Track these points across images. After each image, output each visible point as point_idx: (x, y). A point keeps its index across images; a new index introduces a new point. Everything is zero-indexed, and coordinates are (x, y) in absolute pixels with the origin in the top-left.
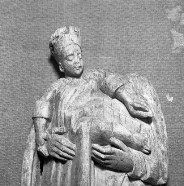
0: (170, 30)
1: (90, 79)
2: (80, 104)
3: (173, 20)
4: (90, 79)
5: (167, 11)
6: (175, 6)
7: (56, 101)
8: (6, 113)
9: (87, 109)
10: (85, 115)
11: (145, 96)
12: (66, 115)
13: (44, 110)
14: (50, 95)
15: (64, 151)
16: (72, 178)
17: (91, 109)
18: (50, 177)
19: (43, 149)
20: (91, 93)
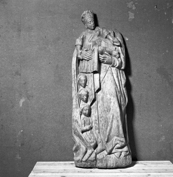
0: (128, 11)
1: (97, 31)
2: (94, 40)
3: (129, 7)
4: (97, 31)
5: (127, 3)
6: (130, 1)
7: (83, 40)
8: (64, 44)
9: (97, 42)
10: (96, 44)
11: (117, 38)
12: (108, 165)
13: (79, 42)
14: (82, 37)
15: (89, 57)
16: (126, 136)
17: (98, 42)
18: (83, 67)
19: (79, 56)
20: (98, 36)
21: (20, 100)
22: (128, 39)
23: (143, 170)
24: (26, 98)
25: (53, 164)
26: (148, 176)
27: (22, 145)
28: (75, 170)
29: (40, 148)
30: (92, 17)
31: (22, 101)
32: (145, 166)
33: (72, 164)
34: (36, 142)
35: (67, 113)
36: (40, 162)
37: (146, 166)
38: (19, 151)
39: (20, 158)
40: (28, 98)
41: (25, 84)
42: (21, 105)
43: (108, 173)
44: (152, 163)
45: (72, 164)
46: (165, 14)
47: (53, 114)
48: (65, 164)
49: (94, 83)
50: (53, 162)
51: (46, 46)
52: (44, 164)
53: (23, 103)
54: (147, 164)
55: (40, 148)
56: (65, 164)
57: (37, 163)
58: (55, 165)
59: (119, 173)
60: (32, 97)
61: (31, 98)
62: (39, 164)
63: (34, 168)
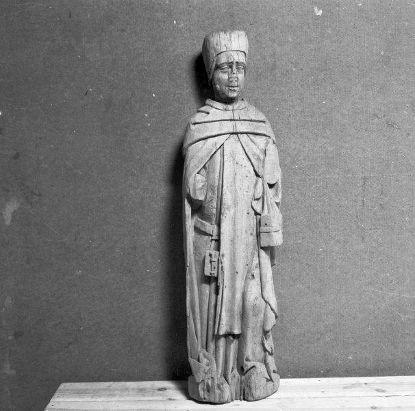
25: (105, 390)
30: (218, 67)
32: (379, 394)
36: (68, 384)
37: (383, 394)
39: (13, 372)
41: (17, 156)
42: (8, 222)
43: (250, 161)
44: (352, 386)
45: (160, 390)
49: (214, 121)
50: (107, 384)
52: (352, 386)
53: (14, 214)
55: (70, 343)
57: (62, 386)
59: (209, 329)
60: (40, 195)
62: (64, 393)
63: (49, 405)
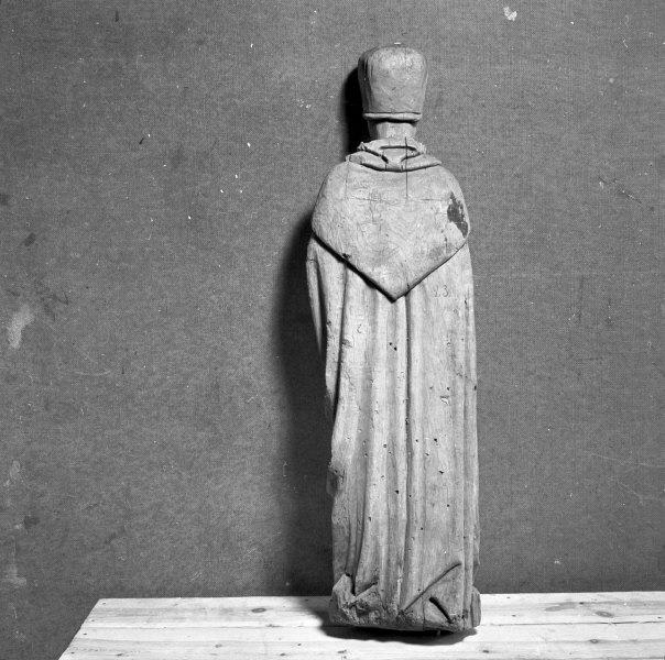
21: (8, 319)
22: (515, 14)
23: (594, 646)
24: (39, 309)
26: (283, 658)
27: (29, 522)
28: (265, 644)
29: (113, 536)
31: (18, 324)
33: (256, 611)
34: (89, 508)
35: (230, 374)
38: (18, 549)
39: (22, 581)
40: (47, 310)
42: (16, 344)
45: (256, 611)
46: (513, 16)
47: (163, 381)
48: (226, 612)
50: (197, 600)
51: (122, 60)
53: (25, 331)
54: (612, 609)
55: (113, 536)
56: (226, 612)
57: (100, 604)
58: (152, 615)
61: (62, 307)
